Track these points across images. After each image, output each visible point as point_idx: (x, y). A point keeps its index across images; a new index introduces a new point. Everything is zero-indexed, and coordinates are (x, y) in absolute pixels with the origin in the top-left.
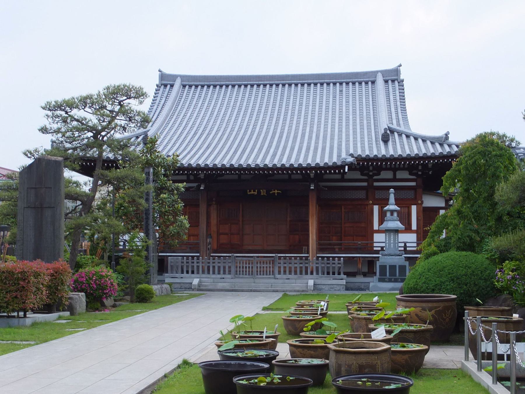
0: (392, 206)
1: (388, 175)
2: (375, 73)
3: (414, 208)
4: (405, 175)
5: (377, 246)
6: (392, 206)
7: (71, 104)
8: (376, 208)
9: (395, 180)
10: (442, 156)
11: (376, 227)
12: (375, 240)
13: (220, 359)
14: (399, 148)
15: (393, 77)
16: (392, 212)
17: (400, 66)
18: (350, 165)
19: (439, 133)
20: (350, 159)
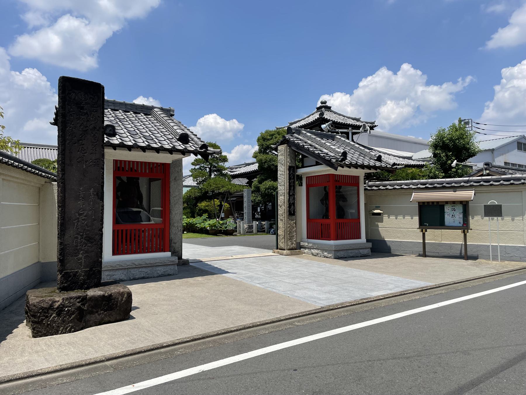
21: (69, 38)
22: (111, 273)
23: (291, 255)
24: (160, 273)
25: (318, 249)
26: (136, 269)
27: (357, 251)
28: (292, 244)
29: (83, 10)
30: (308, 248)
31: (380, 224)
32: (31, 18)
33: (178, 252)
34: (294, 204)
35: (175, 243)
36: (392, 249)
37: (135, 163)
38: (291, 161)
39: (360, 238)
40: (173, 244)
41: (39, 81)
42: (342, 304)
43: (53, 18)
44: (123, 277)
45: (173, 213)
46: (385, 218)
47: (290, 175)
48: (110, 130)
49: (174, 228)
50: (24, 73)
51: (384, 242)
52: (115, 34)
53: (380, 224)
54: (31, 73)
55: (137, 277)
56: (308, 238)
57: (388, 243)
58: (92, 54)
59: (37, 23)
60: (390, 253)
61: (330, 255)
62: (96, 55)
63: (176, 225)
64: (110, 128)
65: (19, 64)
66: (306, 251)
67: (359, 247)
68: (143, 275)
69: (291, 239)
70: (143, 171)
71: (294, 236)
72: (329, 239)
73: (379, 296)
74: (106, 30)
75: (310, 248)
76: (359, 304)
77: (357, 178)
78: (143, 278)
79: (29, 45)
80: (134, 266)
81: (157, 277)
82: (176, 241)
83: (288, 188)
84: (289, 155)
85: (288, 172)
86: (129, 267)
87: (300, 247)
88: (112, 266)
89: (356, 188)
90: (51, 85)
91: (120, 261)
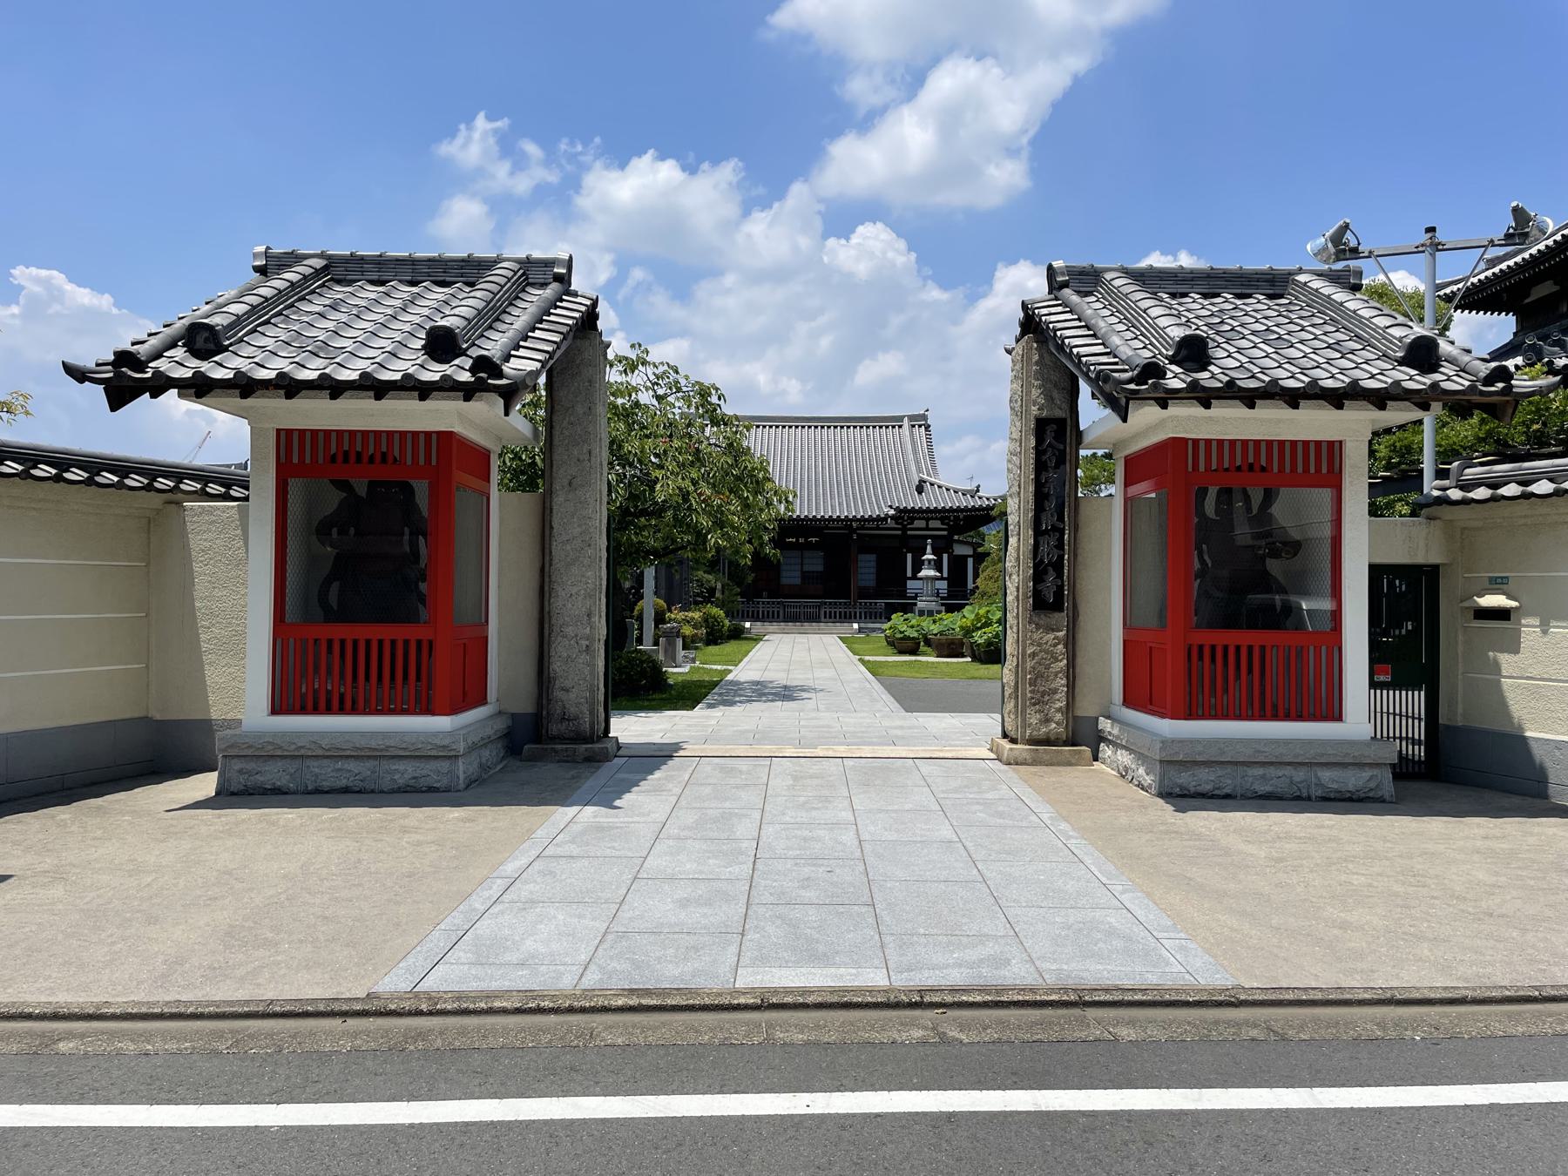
0: (929, 556)
1: (922, 524)
2: (901, 419)
3: (945, 556)
4: (937, 524)
5: (910, 593)
6: (929, 556)
7: (1060, 575)
8: (909, 556)
9: (927, 529)
10: (981, 508)
11: (909, 574)
14: (931, 500)
15: (920, 421)
17: (78, 374)
18: (892, 517)
19: (971, 486)
20: (892, 512)
21: (950, 120)
22: (251, 766)
23: (1035, 762)
24: (401, 782)
26: (326, 762)
27: (1299, 775)
28: (1047, 721)
29: (987, 33)
31: (1505, 659)
32: (859, 89)
34: (1058, 566)
36: (1552, 779)
37: (397, 437)
38: (1049, 398)
39: (1339, 718)
40: (558, 694)
41: (890, 255)
42: (459, 996)
43: (913, 80)
44: (283, 781)
46: (1529, 629)
47: (1039, 451)
48: (206, 340)
50: (855, 240)
51: (1519, 743)
52: (1078, 81)
53: (1505, 659)
54: (873, 238)
55: (326, 785)
56: (1128, 702)
57: (1538, 753)
58: (1011, 152)
59: (876, 100)
60: (1545, 796)
62: (1025, 154)
63: (570, 630)
64: (206, 334)
65: (841, 219)
67: (1344, 757)
68: (344, 783)
70: (295, 460)
71: (1055, 691)
73: (806, 991)
74: (1049, 78)
76: (605, 1010)
77: (1332, 451)
78: (346, 790)
79: (857, 163)
80: (320, 752)
81: (393, 791)
82: (568, 684)
83: (1031, 505)
84: (1039, 375)
85: (1033, 443)
86: (302, 752)
87: (1081, 738)
88: (250, 747)
89: (1326, 494)
90: (918, 261)
91: (275, 734)
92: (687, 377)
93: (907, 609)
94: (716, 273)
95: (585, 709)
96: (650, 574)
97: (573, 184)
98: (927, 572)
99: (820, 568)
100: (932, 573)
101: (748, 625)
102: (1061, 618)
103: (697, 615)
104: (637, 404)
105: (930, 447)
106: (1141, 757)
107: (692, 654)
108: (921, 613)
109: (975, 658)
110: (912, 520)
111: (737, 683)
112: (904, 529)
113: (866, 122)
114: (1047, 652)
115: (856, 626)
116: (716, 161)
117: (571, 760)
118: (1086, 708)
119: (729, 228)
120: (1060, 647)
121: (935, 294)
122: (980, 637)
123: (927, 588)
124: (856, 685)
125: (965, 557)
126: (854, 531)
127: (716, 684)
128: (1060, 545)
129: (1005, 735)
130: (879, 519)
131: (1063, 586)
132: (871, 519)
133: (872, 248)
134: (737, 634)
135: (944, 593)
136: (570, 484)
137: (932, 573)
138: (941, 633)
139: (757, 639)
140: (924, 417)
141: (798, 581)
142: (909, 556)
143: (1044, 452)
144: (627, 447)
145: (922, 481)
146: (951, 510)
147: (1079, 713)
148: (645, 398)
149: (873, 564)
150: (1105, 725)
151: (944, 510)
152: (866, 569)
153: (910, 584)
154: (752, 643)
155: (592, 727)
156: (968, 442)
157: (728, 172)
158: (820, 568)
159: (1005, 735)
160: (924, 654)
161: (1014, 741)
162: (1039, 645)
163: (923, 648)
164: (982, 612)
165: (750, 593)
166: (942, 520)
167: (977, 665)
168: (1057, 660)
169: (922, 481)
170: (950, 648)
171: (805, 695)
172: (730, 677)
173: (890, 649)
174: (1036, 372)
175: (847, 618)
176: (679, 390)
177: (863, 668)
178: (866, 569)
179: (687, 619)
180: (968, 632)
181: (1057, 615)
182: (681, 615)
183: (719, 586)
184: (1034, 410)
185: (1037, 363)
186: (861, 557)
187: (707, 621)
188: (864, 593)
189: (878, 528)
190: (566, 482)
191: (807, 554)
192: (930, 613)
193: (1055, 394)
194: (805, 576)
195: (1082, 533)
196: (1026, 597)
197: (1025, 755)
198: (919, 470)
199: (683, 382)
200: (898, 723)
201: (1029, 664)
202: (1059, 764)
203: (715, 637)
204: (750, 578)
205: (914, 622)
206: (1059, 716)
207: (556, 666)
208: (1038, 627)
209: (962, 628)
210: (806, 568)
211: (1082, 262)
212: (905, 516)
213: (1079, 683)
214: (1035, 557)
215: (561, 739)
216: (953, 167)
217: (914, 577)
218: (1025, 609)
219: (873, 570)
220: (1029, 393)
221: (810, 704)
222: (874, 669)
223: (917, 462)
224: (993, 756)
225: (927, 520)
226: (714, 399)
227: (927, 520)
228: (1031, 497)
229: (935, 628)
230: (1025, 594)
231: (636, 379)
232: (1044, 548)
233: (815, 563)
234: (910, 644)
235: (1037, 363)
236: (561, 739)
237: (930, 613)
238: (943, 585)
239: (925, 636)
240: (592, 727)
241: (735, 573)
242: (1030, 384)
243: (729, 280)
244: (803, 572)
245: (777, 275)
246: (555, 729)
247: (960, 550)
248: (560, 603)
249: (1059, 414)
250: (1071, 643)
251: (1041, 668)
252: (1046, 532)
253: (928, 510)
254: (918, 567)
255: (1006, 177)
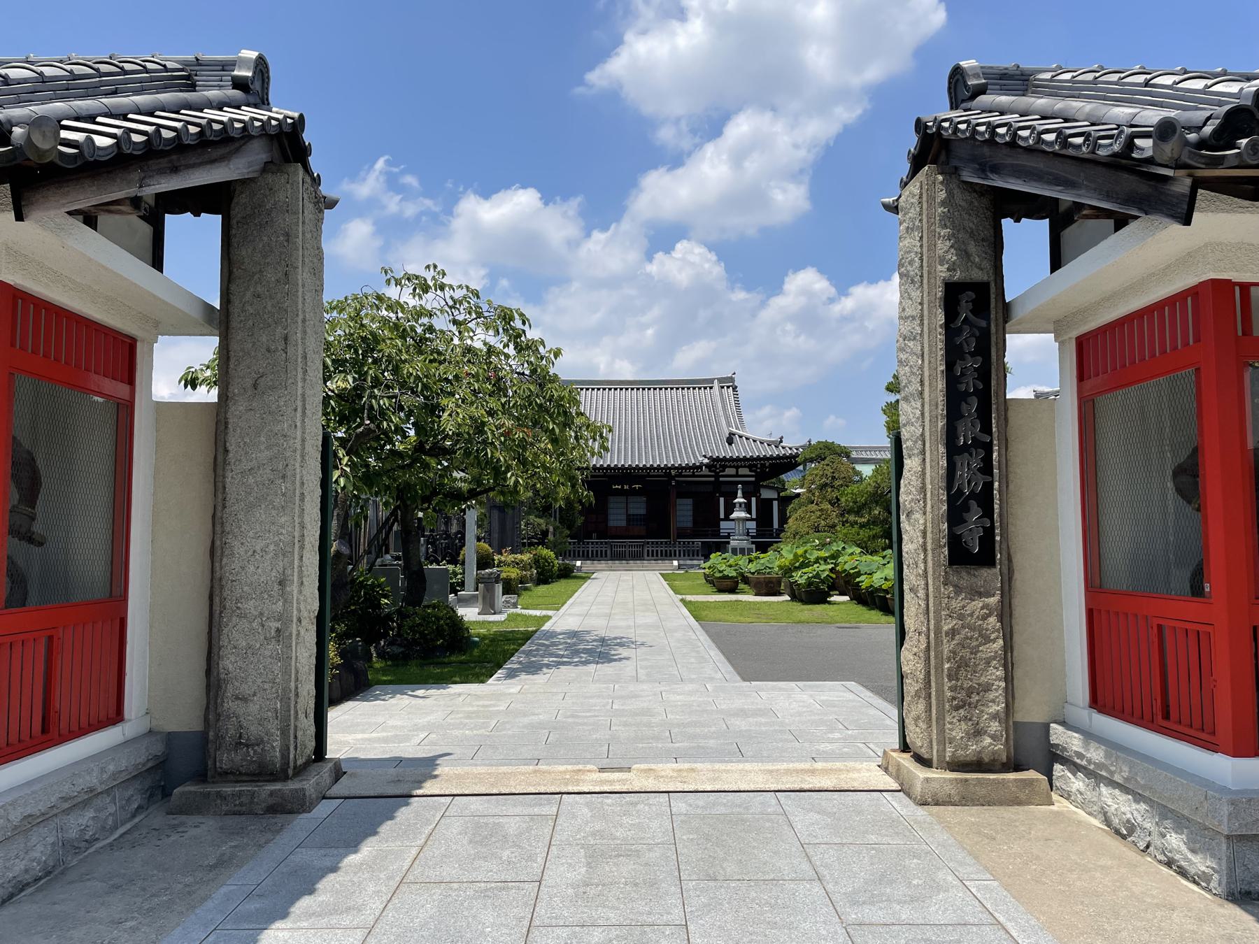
0: (740, 500)
1: (732, 471)
2: (712, 381)
3: (754, 499)
5: (723, 532)
6: (740, 500)
7: (988, 512)
8: (722, 500)
9: (737, 475)
10: (784, 457)
11: (722, 516)
12: (644, 505)
13: (215, 341)
16: (740, 504)
18: (707, 466)
19: (775, 438)
20: (706, 461)
23: (965, 800)
25: (1138, 798)
28: (978, 733)
30: (1089, 774)
33: (260, 742)
34: (985, 499)
35: (245, 700)
38: (964, 254)
40: (230, 705)
43: (711, 127)
45: (239, 550)
49: (244, 624)
61: (1200, 863)
63: (250, 606)
65: (662, 238)
66: (1077, 783)
69: (966, 701)
71: (987, 688)
72: (1206, 739)
74: (819, 129)
75: (1094, 775)
82: (245, 689)
83: (941, 409)
85: (941, 318)
87: (1029, 755)
92: (490, 303)
93: (721, 547)
94: (562, 281)
95: (274, 727)
96: (472, 517)
97: (449, 210)
98: (738, 514)
99: (643, 512)
100: (743, 514)
101: (578, 563)
102: (990, 576)
103: (526, 557)
104: (430, 329)
105: (739, 414)
106: (1200, 838)
107: (512, 598)
108: (734, 551)
109: (794, 597)
110: (724, 468)
111: (552, 634)
112: (717, 476)
113: (676, 161)
114: (972, 629)
115: (675, 563)
116: (565, 198)
117: (245, 810)
118: (1031, 711)
119: (573, 244)
120: (993, 619)
121: (740, 295)
122: (800, 577)
123: (740, 528)
124: (678, 635)
125: (771, 500)
126: (673, 478)
127: (527, 636)
128: (987, 468)
129: (905, 748)
130: (694, 467)
131: (993, 527)
132: (688, 467)
133: (688, 263)
134: (566, 573)
135: (753, 532)
136: (255, 386)
137: (743, 514)
138: (758, 572)
139: (585, 579)
140: (731, 379)
141: (624, 524)
142: (722, 500)
143: (959, 331)
144: (406, 369)
145: (732, 434)
146: (758, 458)
147: (1019, 717)
148: (441, 323)
149: (690, 507)
150: (1058, 734)
151: (752, 459)
152: (683, 512)
153: (723, 524)
154: (580, 582)
155: (285, 756)
156: (767, 410)
157: (575, 203)
158: (643, 512)
159: (905, 748)
160: (743, 592)
161: (925, 762)
162: (961, 617)
163: (741, 586)
164: (800, 551)
165: (581, 535)
166: (750, 467)
167: (798, 606)
168: (988, 640)
169: (732, 434)
170: (769, 587)
171: (624, 652)
172: (547, 627)
173: (709, 588)
174: (943, 217)
175: (668, 556)
176: (479, 315)
177: (685, 611)
178: (683, 512)
179: (511, 563)
180: (788, 571)
181: (985, 573)
182: (511, 558)
183: (551, 529)
184: (942, 272)
185: (943, 203)
186: (679, 501)
187: (537, 561)
188: (682, 534)
189: (693, 476)
190: (249, 382)
191: (631, 499)
192: (742, 551)
193: (972, 248)
194: (630, 519)
195: (1013, 446)
196: (938, 546)
197: (949, 789)
198: (729, 424)
199: (485, 307)
200: (738, 703)
201: (946, 649)
202: (1001, 803)
203: (545, 576)
204: (580, 521)
205: (732, 561)
206: (995, 726)
207: (229, 663)
208: (958, 590)
209: (781, 567)
210: (631, 512)
211: (1005, 62)
212: (717, 464)
213: (1018, 673)
214: (949, 487)
215: (228, 775)
216: (748, 198)
217: (727, 518)
218: (937, 564)
219: (691, 513)
220: (932, 247)
221: (628, 668)
222: (696, 611)
223: (727, 418)
224: (895, 786)
225: (737, 468)
226: (518, 323)
227: (737, 468)
228: (941, 399)
229: (752, 567)
230: (936, 542)
231: (431, 300)
232: (963, 473)
233: (639, 507)
234: (728, 583)
235: (943, 203)
236: (228, 775)
237: (742, 551)
238: (752, 525)
239: (742, 575)
240: (285, 756)
241: (565, 516)
242: (932, 233)
243: (576, 286)
244: (628, 516)
245: (612, 283)
246: (225, 759)
247: (766, 494)
248: (236, 565)
249: (977, 275)
250: (1005, 613)
251: (965, 653)
252: (966, 448)
253: (738, 459)
254: (730, 508)
255: (789, 199)
